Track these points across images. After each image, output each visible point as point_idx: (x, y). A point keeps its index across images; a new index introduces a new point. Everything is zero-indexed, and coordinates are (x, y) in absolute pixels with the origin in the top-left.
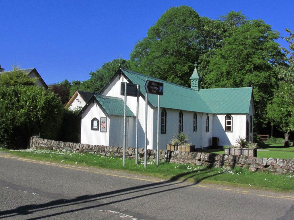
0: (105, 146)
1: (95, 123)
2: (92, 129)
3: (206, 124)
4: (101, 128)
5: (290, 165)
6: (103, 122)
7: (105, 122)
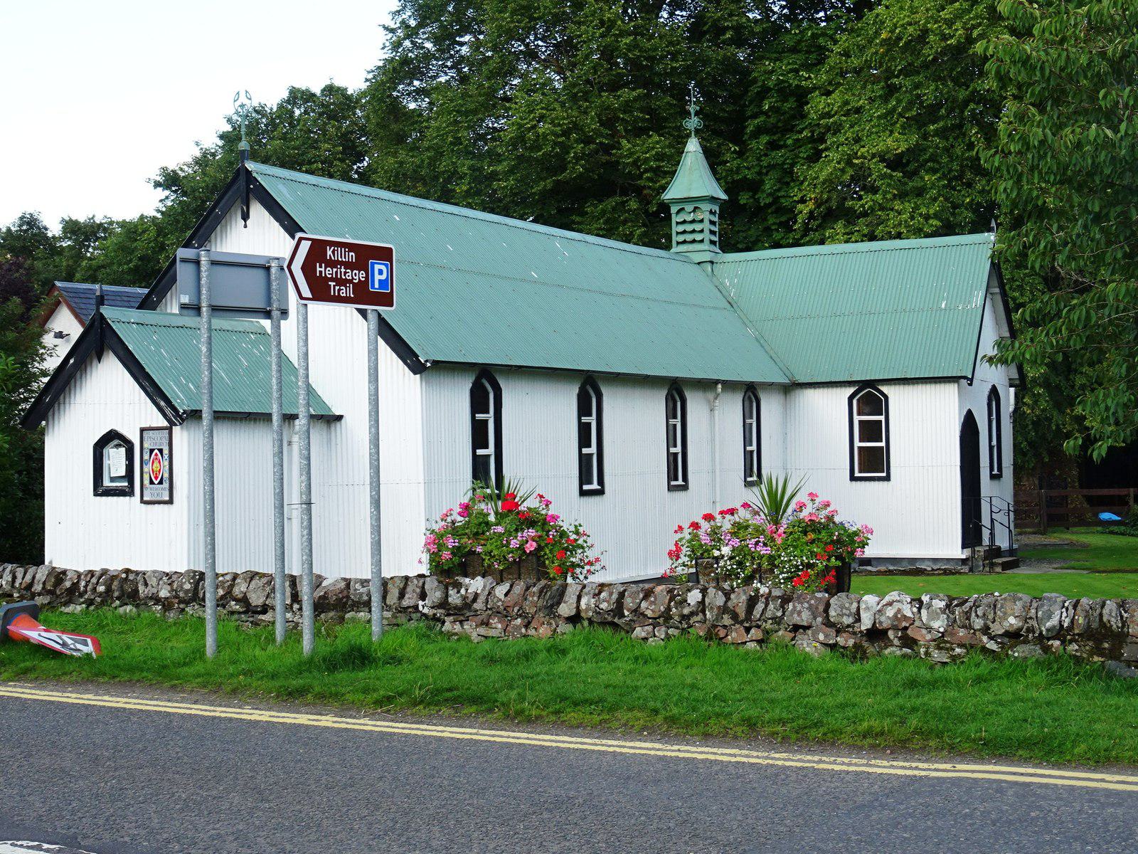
0: (137, 573)
1: (115, 461)
2: (100, 490)
3: (747, 441)
4: (146, 482)
5: (978, 623)
6: (152, 451)
7: (166, 452)
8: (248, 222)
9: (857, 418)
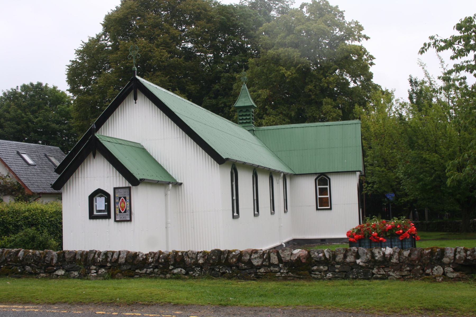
1: (100, 203)
2: (92, 216)
4: (117, 212)
6: (120, 198)
7: (128, 198)
8: (137, 101)
9: (318, 187)
